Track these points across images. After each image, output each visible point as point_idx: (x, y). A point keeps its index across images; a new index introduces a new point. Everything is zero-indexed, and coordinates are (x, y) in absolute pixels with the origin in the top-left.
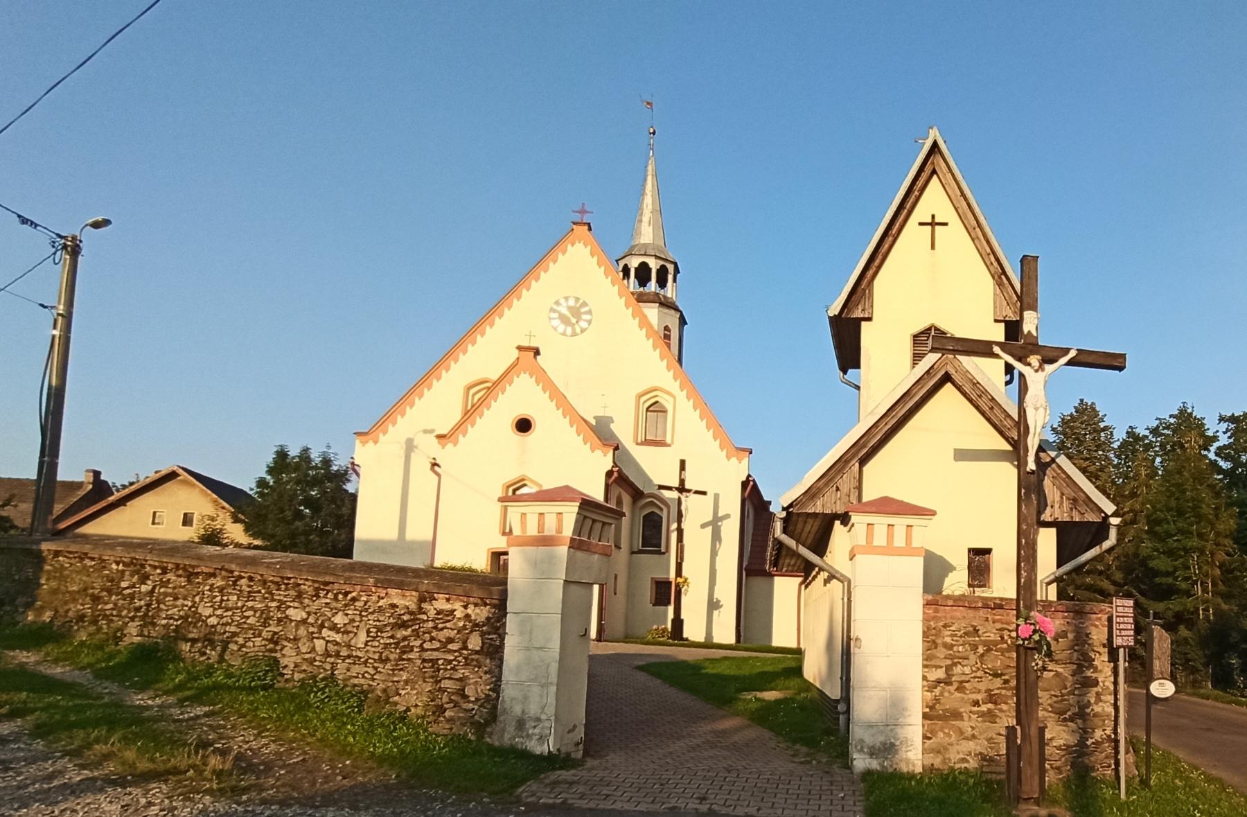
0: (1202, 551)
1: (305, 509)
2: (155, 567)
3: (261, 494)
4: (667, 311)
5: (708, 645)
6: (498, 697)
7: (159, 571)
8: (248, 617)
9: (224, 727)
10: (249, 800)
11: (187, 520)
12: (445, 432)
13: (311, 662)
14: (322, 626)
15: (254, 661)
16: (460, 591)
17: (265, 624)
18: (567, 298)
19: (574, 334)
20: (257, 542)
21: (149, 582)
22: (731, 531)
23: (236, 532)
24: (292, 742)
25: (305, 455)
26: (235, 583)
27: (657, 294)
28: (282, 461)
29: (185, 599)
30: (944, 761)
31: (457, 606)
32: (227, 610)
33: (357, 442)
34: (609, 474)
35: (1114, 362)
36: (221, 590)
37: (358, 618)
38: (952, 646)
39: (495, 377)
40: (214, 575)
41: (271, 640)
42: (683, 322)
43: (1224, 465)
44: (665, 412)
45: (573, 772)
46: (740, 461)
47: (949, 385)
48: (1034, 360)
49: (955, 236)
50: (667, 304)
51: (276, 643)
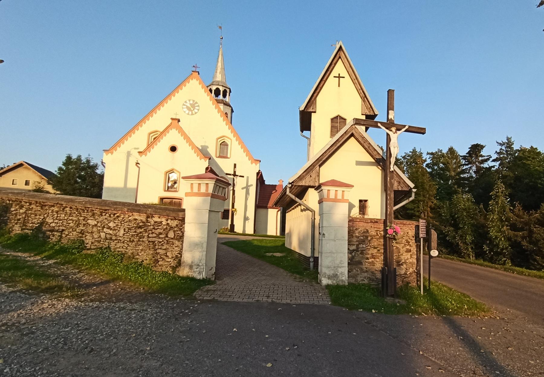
0: (424, 201)
1: (80, 179)
2: (26, 202)
3: (60, 173)
4: (226, 107)
5: (244, 234)
6: (181, 257)
7: (28, 204)
8: (70, 223)
9: (63, 269)
10: (85, 300)
11: (27, 183)
12: (142, 151)
13: (99, 242)
14: (104, 227)
15: (74, 242)
16: (165, 214)
17: (78, 226)
18: (189, 100)
19: (192, 114)
20: (58, 192)
21: (24, 209)
22: (253, 190)
23: (49, 188)
24: (94, 274)
25: (79, 158)
26: (63, 209)
27: (223, 100)
28: (69, 161)
29: (40, 215)
30: (356, 281)
31: (164, 220)
32: (60, 220)
33: (104, 154)
34: (207, 169)
35: (421, 131)
36: (57, 212)
37: (120, 224)
38: (359, 237)
39: (161, 130)
40: (53, 206)
41: (81, 233)
42: (232, 111)
43: (429, 170)
44: (227, 145)
45: (212, 286)
46: (256, 164)
47: (353, 138)
48: (394, 129)
49: (347, 82)
50: (226, 104)
51: (83, 234)
